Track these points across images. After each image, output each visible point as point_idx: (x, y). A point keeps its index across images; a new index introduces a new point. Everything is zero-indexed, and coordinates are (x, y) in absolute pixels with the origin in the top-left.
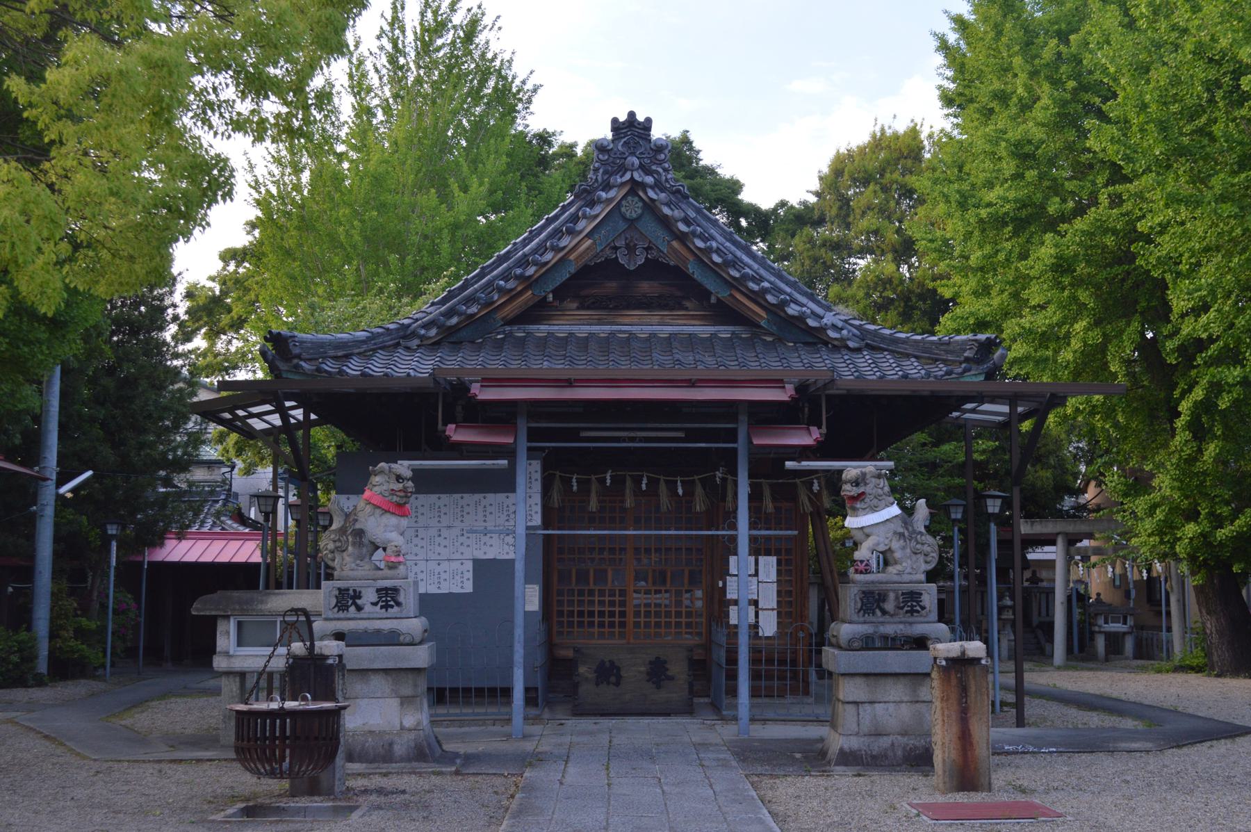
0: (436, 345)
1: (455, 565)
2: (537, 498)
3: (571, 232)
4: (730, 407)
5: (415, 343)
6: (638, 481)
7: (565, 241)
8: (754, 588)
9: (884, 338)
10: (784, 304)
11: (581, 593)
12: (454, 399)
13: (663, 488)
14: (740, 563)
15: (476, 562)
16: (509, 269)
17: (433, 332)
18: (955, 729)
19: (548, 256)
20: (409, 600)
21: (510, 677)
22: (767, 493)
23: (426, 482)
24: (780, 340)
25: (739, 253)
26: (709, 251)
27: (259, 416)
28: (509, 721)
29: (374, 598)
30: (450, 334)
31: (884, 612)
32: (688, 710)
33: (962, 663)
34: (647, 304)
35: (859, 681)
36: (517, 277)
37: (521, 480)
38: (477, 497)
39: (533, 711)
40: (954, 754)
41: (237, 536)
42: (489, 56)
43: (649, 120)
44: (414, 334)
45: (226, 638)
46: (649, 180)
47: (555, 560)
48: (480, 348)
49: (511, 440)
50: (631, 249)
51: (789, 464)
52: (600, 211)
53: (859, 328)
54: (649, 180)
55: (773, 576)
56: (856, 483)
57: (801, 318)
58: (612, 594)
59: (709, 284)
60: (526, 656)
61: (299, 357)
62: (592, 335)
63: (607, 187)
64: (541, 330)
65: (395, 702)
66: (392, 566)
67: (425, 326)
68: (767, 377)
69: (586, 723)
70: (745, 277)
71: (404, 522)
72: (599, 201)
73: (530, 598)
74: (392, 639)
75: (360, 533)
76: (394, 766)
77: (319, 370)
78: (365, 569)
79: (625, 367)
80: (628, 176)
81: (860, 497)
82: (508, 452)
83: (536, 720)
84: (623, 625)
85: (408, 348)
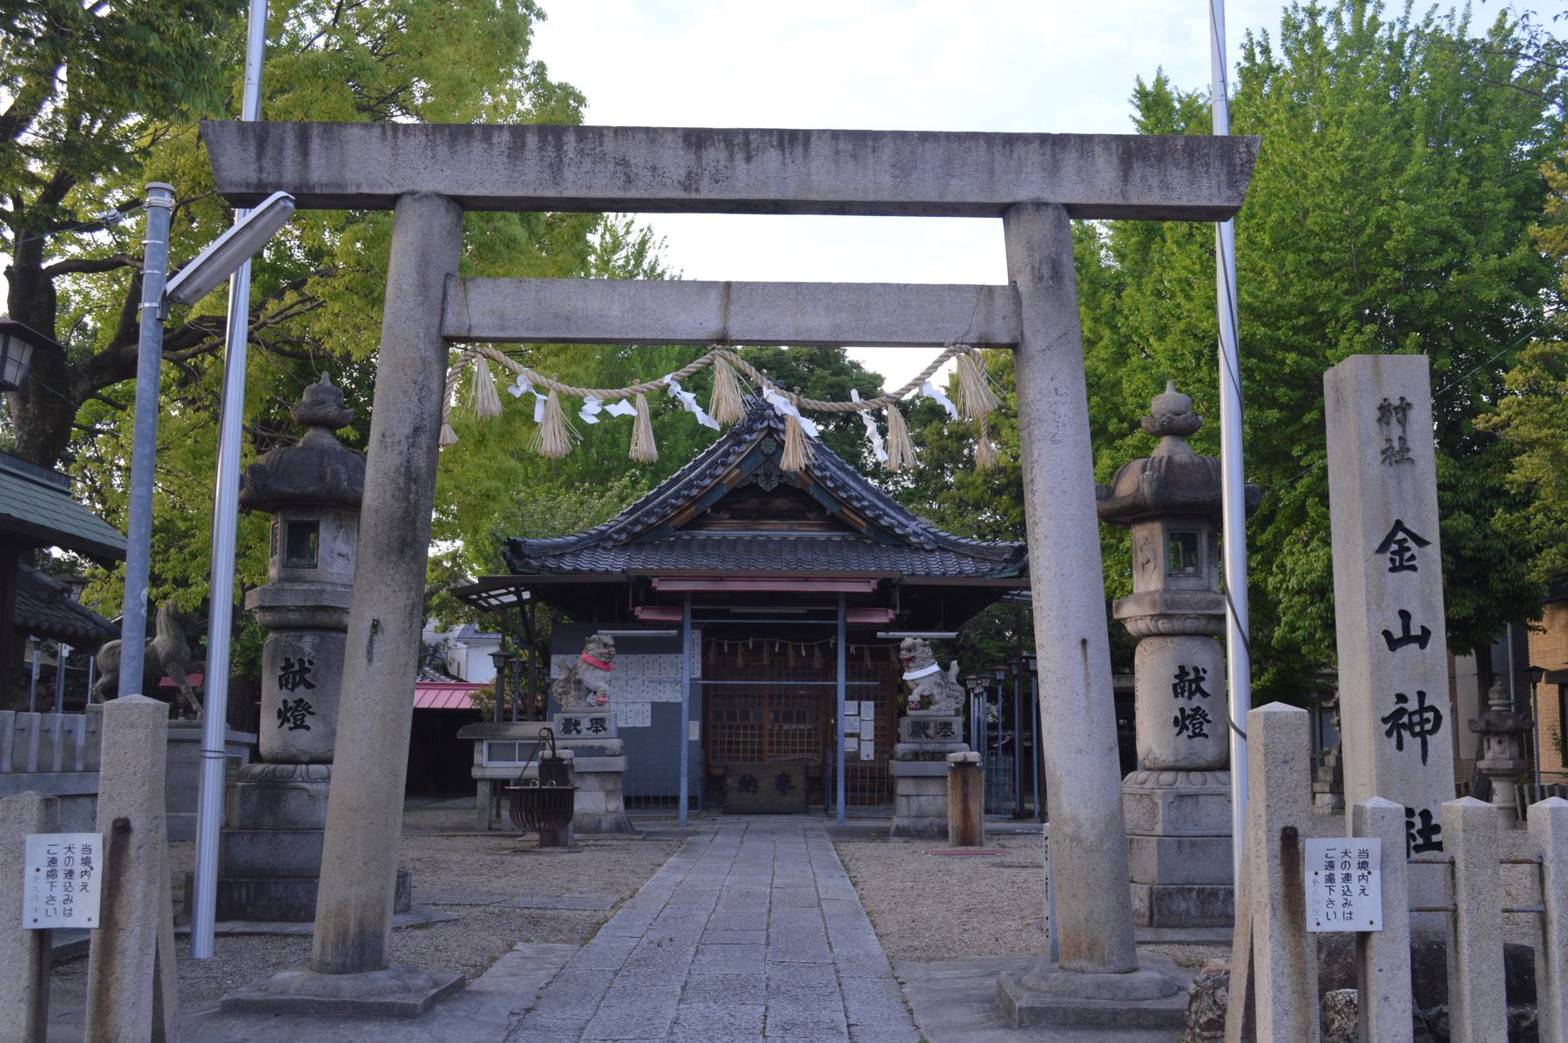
0: (625, 546)
1: (638, 707)
2: (699, 658)
3: (724, 464)
4: (832, 598)
5: (610, 544)
6: (772, 645)
7: (720, 471)
8: (857, 723)
9: (950, 542)
10: (878, 517)
11: (731, 727)
12: (638, 589)
13: (791, 651)
14: (847, 708)
15: (654, 705)
16: (678, 491)
17: (623, 536)
18: (959, 807)
19: (707, 482)
20: (611, 726)
21: (678, 789)
22: (867, 653)
23: (623, 646)
24: (877, 543)
25: (847, 479)
26: (824, 478)
27: (495, 597)
28: (677, 817)
29: (588, 724)
30: (637, 537)
31: (927, 736)
32: (804, 810)
33: (964, 765)
34: (780, 515)
35: (910, 781)
36: (685, 497)
37: (686, 646)
38: (654, 656)
39: (694, 812)
40: (959, 823)
41: (446, 687)
42: (659, 270)
44: (609, 538)
45: (481, 755)
47: (710, 701)
48: (657, 548)
49: (679, 618)
50: (768, 476)
51: (880, 634)
52: (745, 449)
53: (934, 534)
55: (872, 716)
56: (909, 650)
57: (891, 528)
58: (753, 727)
59: (825, 501)
60: (689, 773)
62: (739, 538)
63: (750, 431)
64: (702, 534)
65: (602, 794)
66: (601, 704)
67: (616, 532)
68: (853, 575)
69: (733, 819)
70: (850, 497)
71: (608, 674)
72: (745, 442)
73: (693, 731)
74: (601, 751)
75: (579, 682)
76: (601, 836)
77: (543, 566)
78: (582, 706)
79: (762, 565)
81: (912, 659)
82: (678, 626)
83: (697, 817)
84: (761, 751)
85: (605, 549)
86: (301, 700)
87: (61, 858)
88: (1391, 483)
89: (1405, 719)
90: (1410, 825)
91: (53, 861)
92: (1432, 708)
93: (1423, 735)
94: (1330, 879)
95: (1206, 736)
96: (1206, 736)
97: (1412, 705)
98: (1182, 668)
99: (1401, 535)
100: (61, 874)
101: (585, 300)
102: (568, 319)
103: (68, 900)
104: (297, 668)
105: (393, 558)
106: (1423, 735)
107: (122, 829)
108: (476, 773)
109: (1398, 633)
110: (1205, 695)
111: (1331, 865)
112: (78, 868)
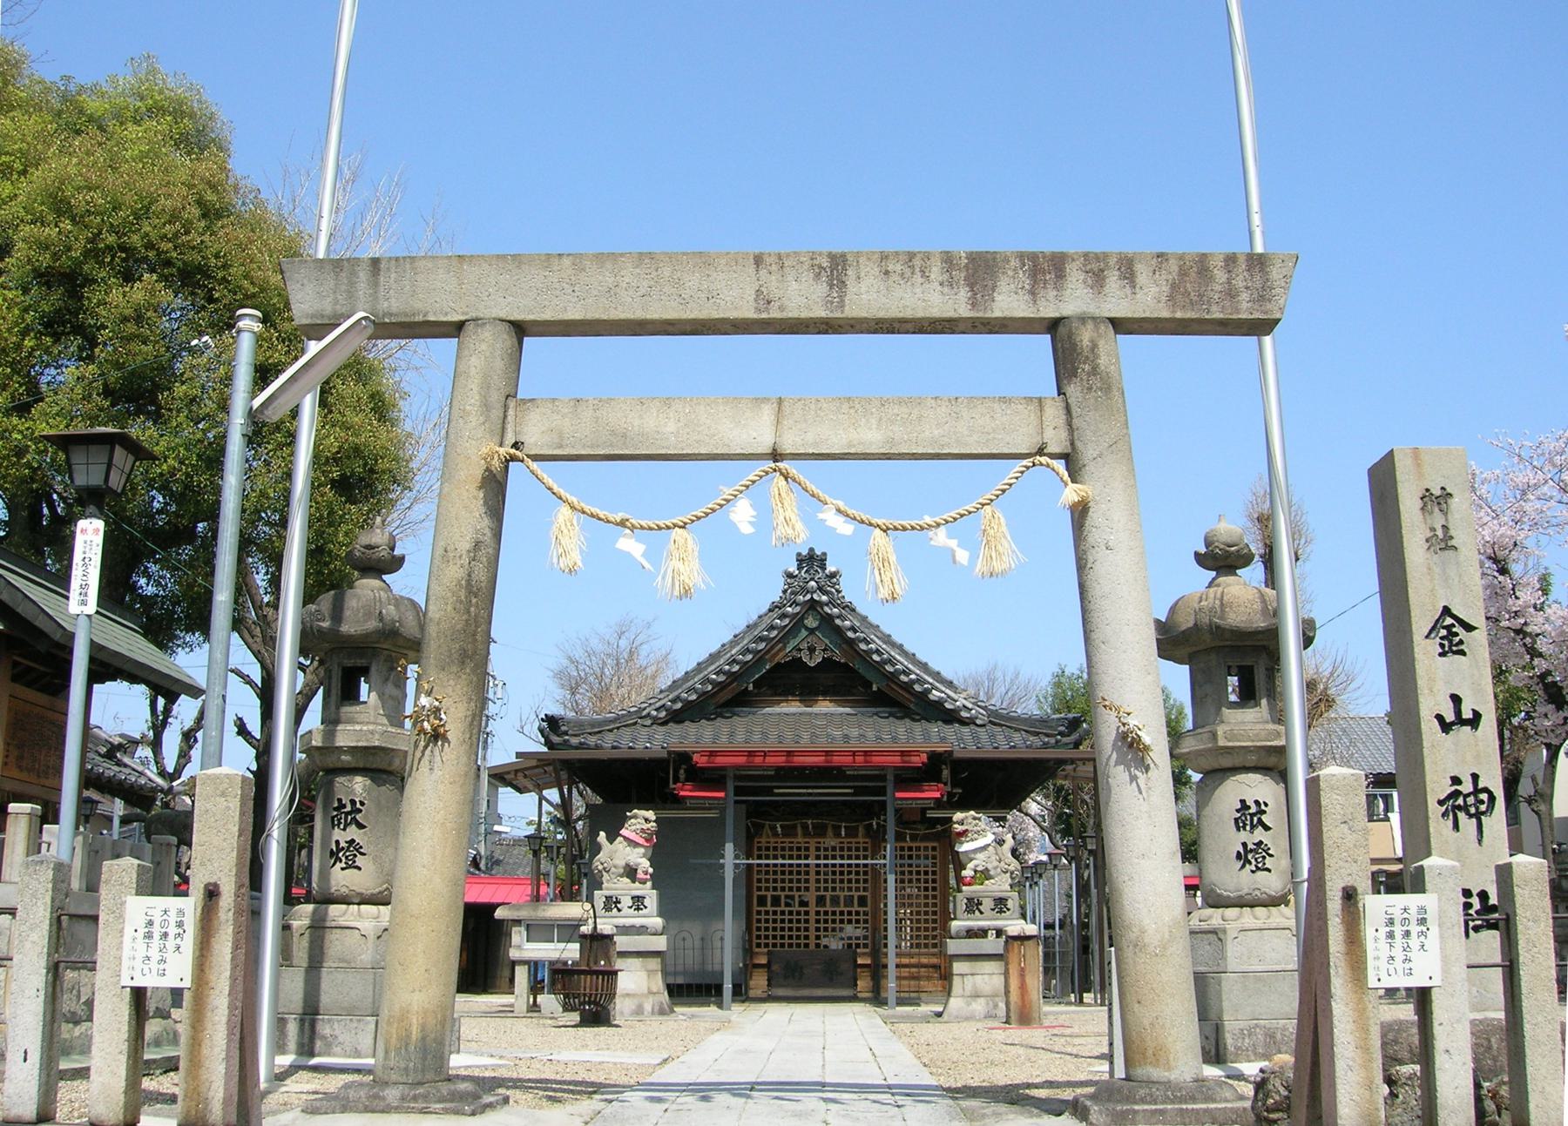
10: (928, 691)
26: (870, 652)
43: (824, 554)
46: (824, 598)
54: (824, 598)
59: (869, 676)
61: (566, 733)
65: (644, 974)
74: (642, 930)
80: (808, 597)
86: (353, 841)
87: (157, 921)
88: (1437, 570)
89: (1460, 801)
90: (1467, 906)
91: (150, 923)
92: (1486, 790)
93: (1478, 816)
94: (1391, 935)
95: (1269, 870)
96: (1269, 870)
97: (1467, 787)
98: (1243, 802)
99: (1449, 621)
100: (157, 936)
101: (641, 417)
102: (624, 436)
103: (162, 961)
104: (349, 808)
105: (454, 669)
106: (1478, 816)
107: (212, 893)
108: (514, 954)
109: (1450, 717)
110: (1267, 828)
111: (1391, 922)
112: (172, 930)
